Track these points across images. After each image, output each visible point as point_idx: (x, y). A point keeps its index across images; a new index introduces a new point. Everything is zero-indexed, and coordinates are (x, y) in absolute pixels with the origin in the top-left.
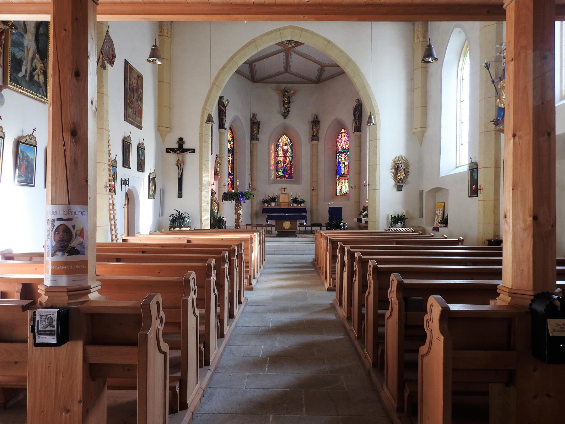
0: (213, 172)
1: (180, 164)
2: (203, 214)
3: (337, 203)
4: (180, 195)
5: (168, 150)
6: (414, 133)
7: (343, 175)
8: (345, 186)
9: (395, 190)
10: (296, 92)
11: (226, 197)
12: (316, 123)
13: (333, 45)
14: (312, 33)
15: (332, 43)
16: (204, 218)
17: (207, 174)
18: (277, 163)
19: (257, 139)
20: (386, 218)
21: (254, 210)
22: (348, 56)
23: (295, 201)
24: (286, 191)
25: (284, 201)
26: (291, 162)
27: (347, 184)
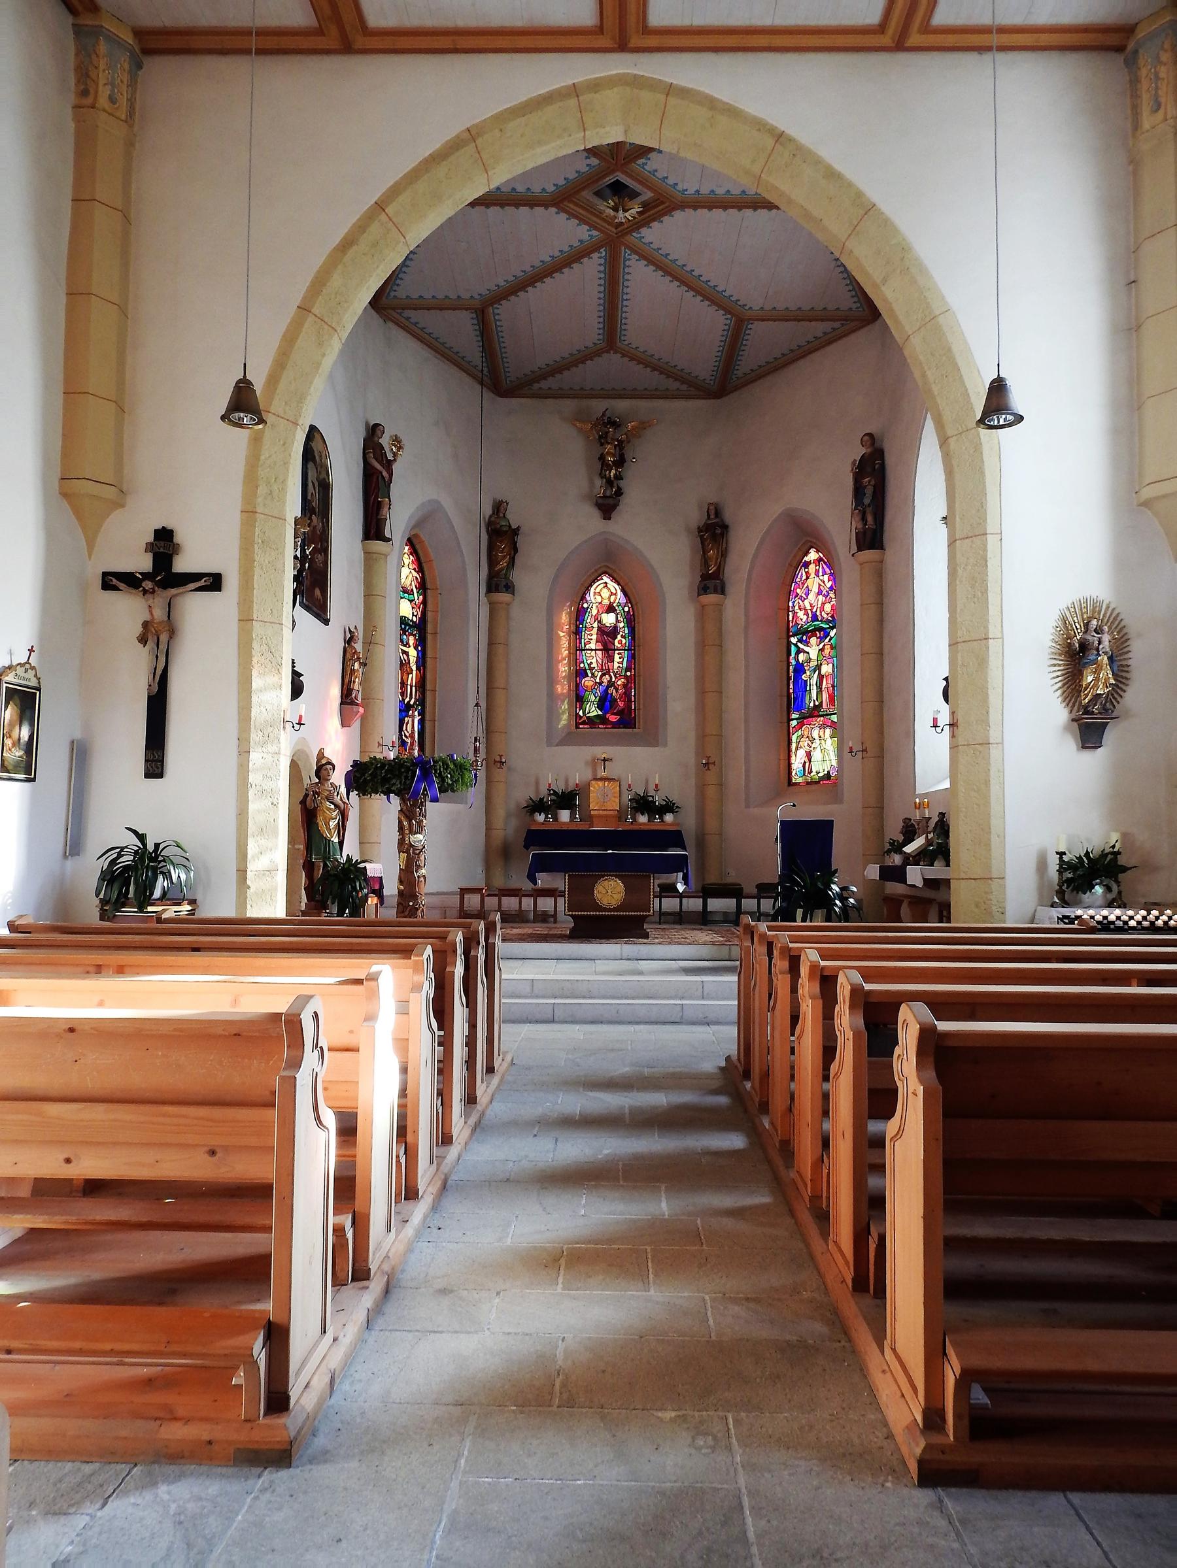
0: (335, 692)
1: (159, 637)
2: (252, 847)
3: (809, 811)
4: (155, 767)
5: (111, 581)
6: (1146, 504)
7: (815, 711)
8: (823, 750)
9: (1070, 744)
10: (644, 426)
11: (368, 777)
12: (713, 532)
13: (800, 152)
14: (711, 103)
15: (791, 140)
16: (254, 867)
17: (272, 679)
18: (581, 673)
19: (509, 588)
20: (1032, 865)
21: (499, 835)
22: (860, 194)
23: (643, 804)
24: (611, 770)
25: (604, 802)
26: (628, 669)
27: (830, 744)
